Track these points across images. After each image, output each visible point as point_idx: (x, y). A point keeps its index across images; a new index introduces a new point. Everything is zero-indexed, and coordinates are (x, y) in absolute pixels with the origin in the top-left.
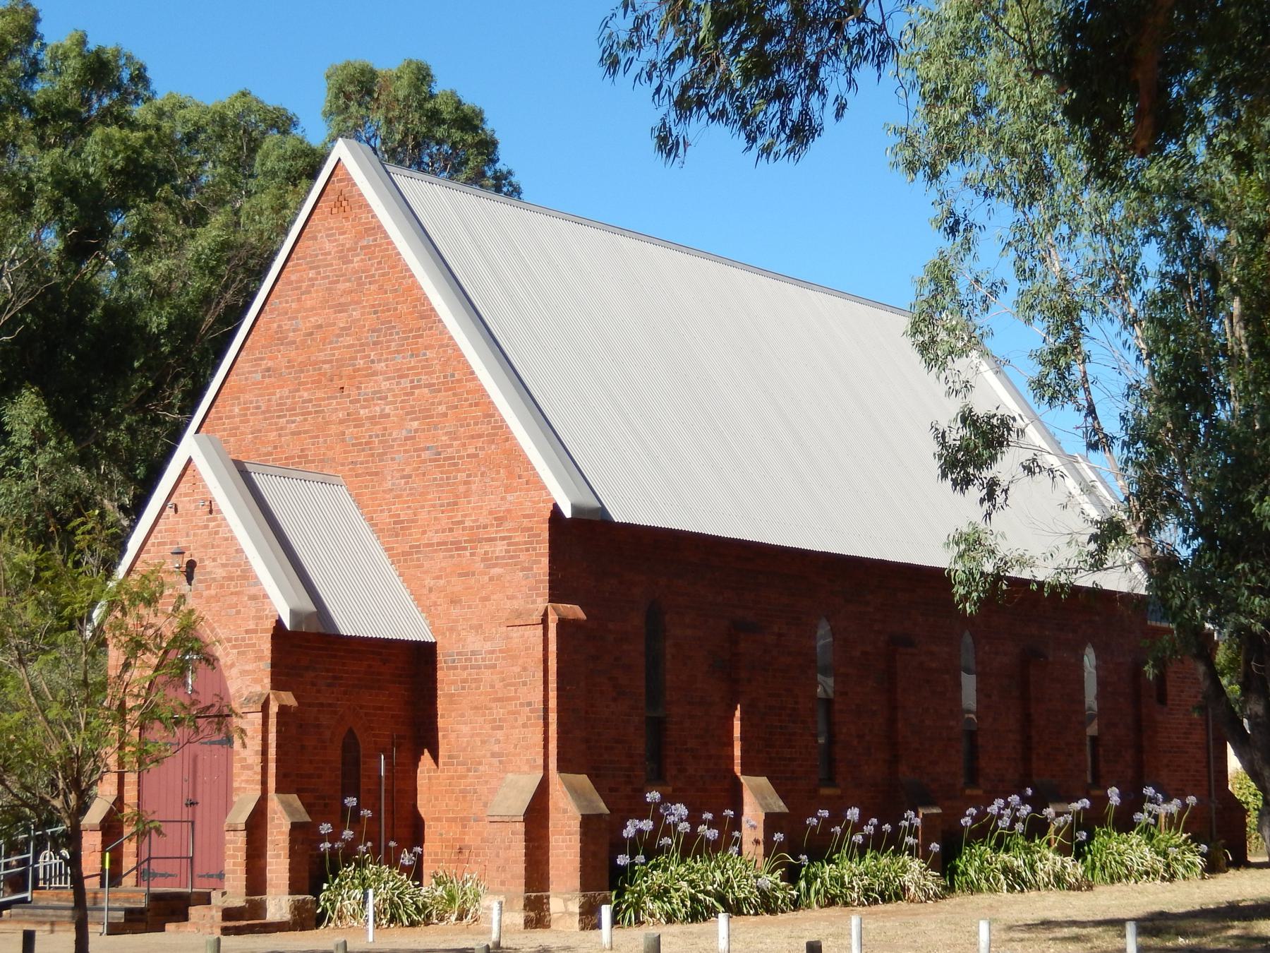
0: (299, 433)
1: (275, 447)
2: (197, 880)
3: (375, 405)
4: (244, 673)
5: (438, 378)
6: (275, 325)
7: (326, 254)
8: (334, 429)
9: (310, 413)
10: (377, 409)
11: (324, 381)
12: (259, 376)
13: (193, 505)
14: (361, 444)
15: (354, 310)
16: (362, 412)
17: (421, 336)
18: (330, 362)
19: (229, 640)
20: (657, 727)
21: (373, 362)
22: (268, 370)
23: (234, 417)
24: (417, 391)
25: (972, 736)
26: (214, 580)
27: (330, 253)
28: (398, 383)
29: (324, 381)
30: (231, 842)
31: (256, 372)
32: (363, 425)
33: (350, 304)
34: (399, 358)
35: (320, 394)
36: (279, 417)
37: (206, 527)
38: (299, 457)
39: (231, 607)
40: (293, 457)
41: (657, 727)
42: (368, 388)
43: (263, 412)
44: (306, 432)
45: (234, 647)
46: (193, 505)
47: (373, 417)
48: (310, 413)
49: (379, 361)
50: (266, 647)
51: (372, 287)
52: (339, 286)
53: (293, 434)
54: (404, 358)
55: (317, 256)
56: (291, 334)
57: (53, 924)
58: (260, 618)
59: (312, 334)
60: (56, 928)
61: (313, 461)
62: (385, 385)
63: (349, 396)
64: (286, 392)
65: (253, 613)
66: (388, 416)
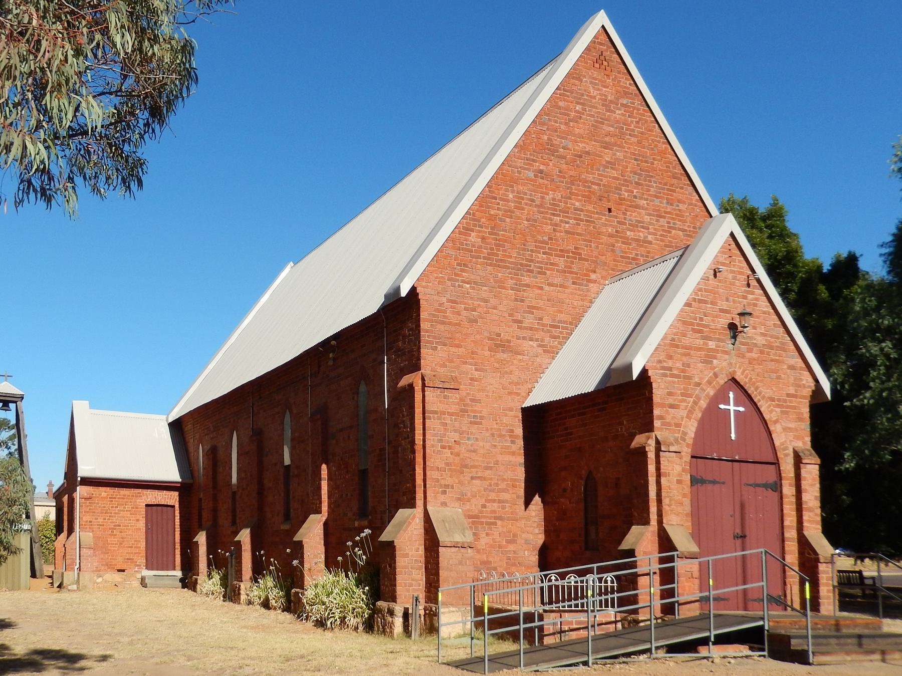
0: (573, 233)
1: (550, 239)
2: (750, 604)
3: (639, 231)
4: (786, 429)
5: (689, 227)
6: (546, 137)
7: (591, 97)
8: (604, 239)
9: (582, 220)
10: (641, 234)
11: (594, 199)
12: (531, 175)
13: (730, 276)
14: (628, 258)
15: (618, 151)
16: (628, 233)
17: (674, 191)
18: (599, 185)
19: (772, 400)
20: (287, 484)
21: (635, 197)
22: (541, 172)
23: (508, 201)
24: (674, 231)
25: (234, 493)
26: (756, 345)
27: (594, 98)
28: (657, 221)
29: (594, 199)
30: (824, 572)
31: (528, 169)
32: (630, 244)
33: (615, 144)
34: (657, 202)
35: (590, 208)
36: (554, 215)
37: (745, 297)
38: (573, 253)
39: (773, 371)
40: (568, 252)
41: (287, 484)
42: (633, 216)
43: (536, 206)
44: (578, 234)
45: (778, 406)
46: (730, 276)
47: (637, 240)
48: (582, 220)
49: (641, 198)
50: (806, 411)
51: (633, 139)
52: (604, 127)
53: (567, 232)
54: (661, 202)
55: (583, 95)
56: (562, 150)
57: (883, 653)
58: (799, 386)
59: (581, 156)
60: (888, 657)
61: (587, 260)
62: (647, 218)
63: (616, 217)
64: (558, 196)
65: (792, 380)
66: (650, 243)
